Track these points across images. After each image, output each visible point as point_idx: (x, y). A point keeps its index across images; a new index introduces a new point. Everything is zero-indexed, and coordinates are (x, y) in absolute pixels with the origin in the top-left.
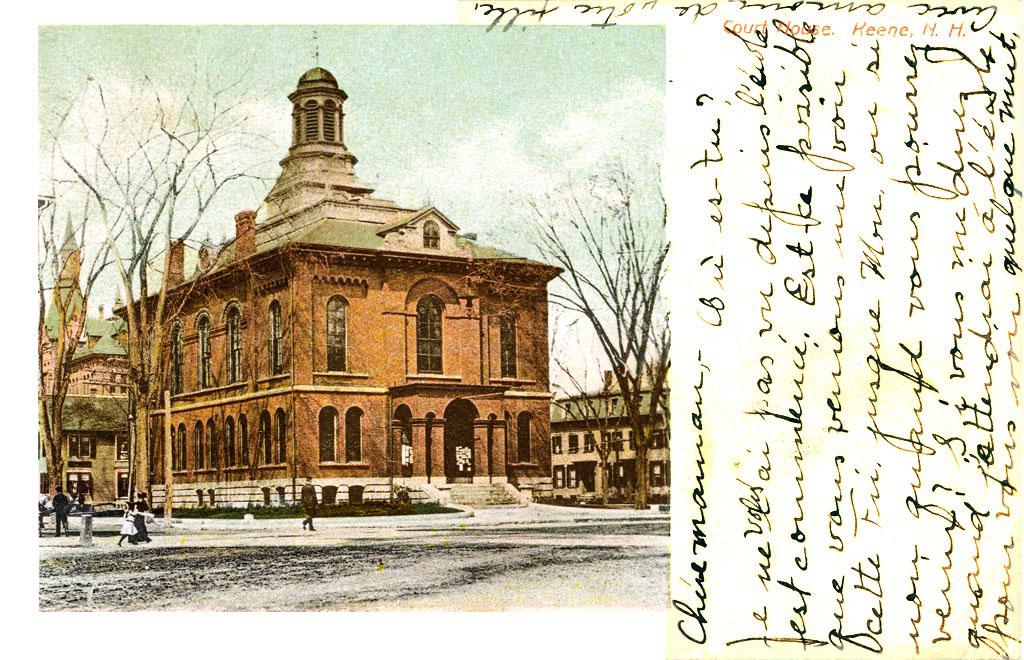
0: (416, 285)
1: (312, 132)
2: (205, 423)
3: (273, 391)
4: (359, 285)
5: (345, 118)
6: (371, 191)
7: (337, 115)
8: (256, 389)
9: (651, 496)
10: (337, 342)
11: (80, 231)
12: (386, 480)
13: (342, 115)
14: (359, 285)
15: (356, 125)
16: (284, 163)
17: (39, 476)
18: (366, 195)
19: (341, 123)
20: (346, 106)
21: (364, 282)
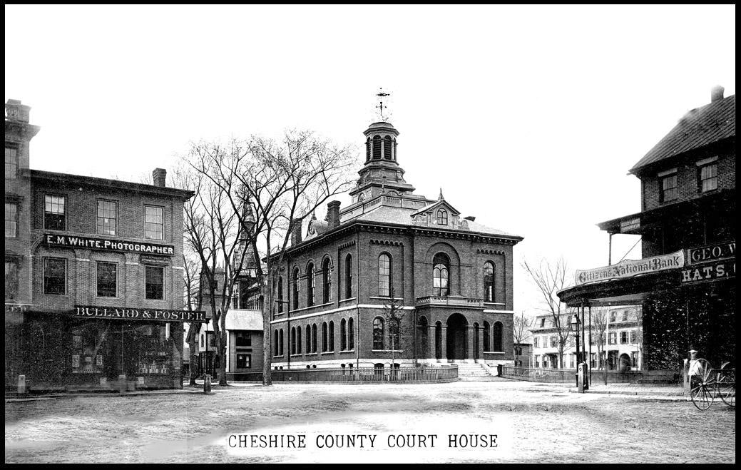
0: (433, 246)
1: (377, 156)
2: (311, 327)
3: (341, 309)
4: (398, 246)
5: (398, 147)
6: (412, 190)
7: (393, 144)
8: (339, 306)
9: (259, 335)
10: (91, 341)
11: (216, 241)
12: (411, 361)
13: (395, 145)
14: (398, 246)
15: (403, 156)
16: (362, 173)
17: (19, 100)
18: (408, 192)
19: (395, 149)
20: (398, 139)
21: (401, 244)
